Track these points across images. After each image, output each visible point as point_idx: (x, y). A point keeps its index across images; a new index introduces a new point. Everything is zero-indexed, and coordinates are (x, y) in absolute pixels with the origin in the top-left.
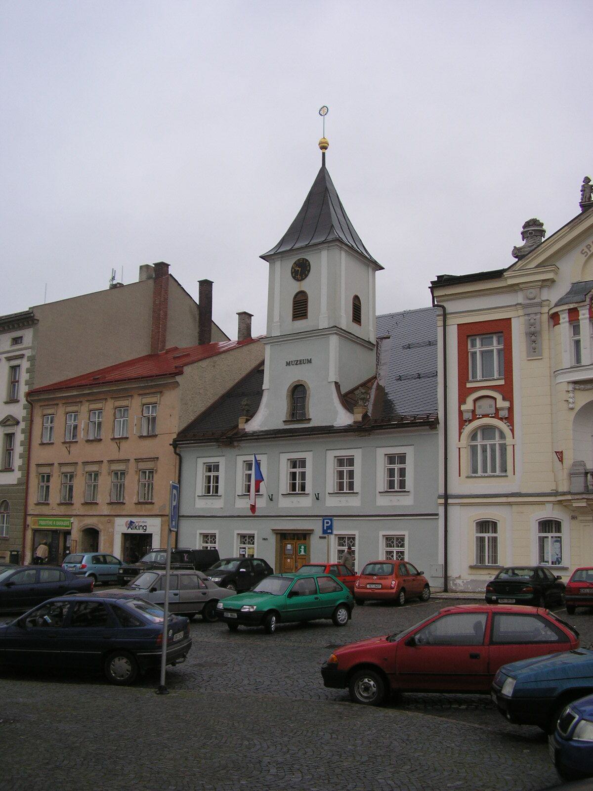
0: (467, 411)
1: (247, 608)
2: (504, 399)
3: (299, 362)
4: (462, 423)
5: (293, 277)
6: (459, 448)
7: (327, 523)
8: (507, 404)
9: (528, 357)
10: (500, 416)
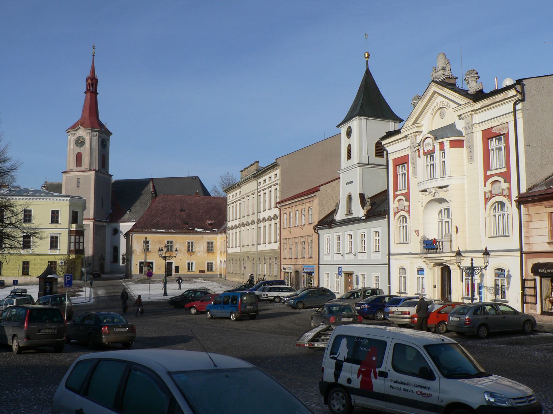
1: (406, 318)
2: (505, 182)
6: (485, 217)
7: (68, 278)
8: (506, 185)
9: (413, 176)
10: (504, 195)
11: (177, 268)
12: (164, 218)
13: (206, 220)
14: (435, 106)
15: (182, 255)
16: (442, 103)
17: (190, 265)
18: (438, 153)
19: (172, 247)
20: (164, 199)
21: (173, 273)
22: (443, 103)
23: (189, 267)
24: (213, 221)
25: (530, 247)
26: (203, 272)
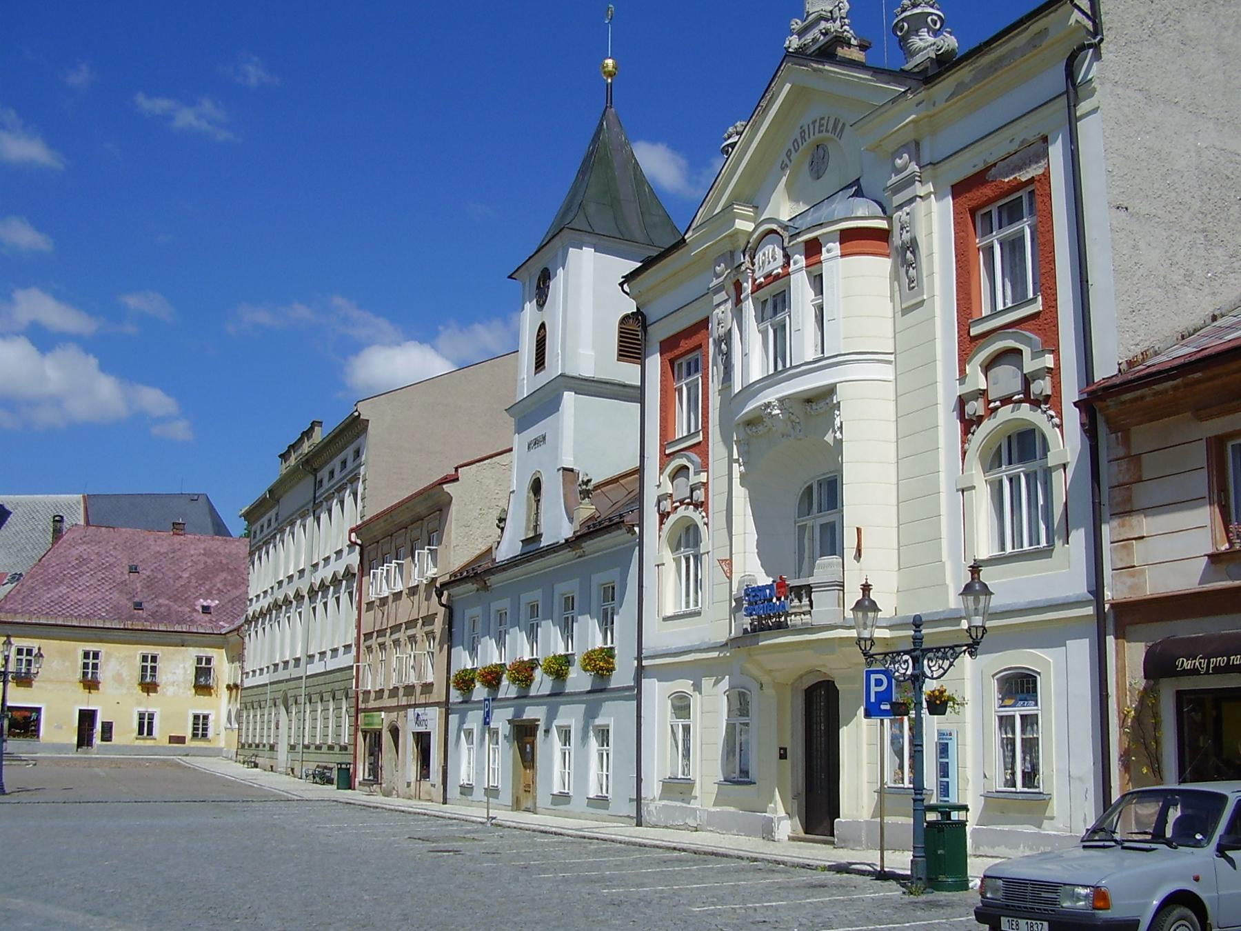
11: (107, 729)
12: (80, 588)
13: (197, 598)
14: (796, 140)
15: (124, 691)
16: (817, 124)
17: (144, 719)
18: (800, 286)
19: (97, 669)
20: (85, 537)
21: (97, 740)
22: (822, 122)
23: (141, 725)
24: (217, 602)
25: (1136, 580)
26: (181, 740)
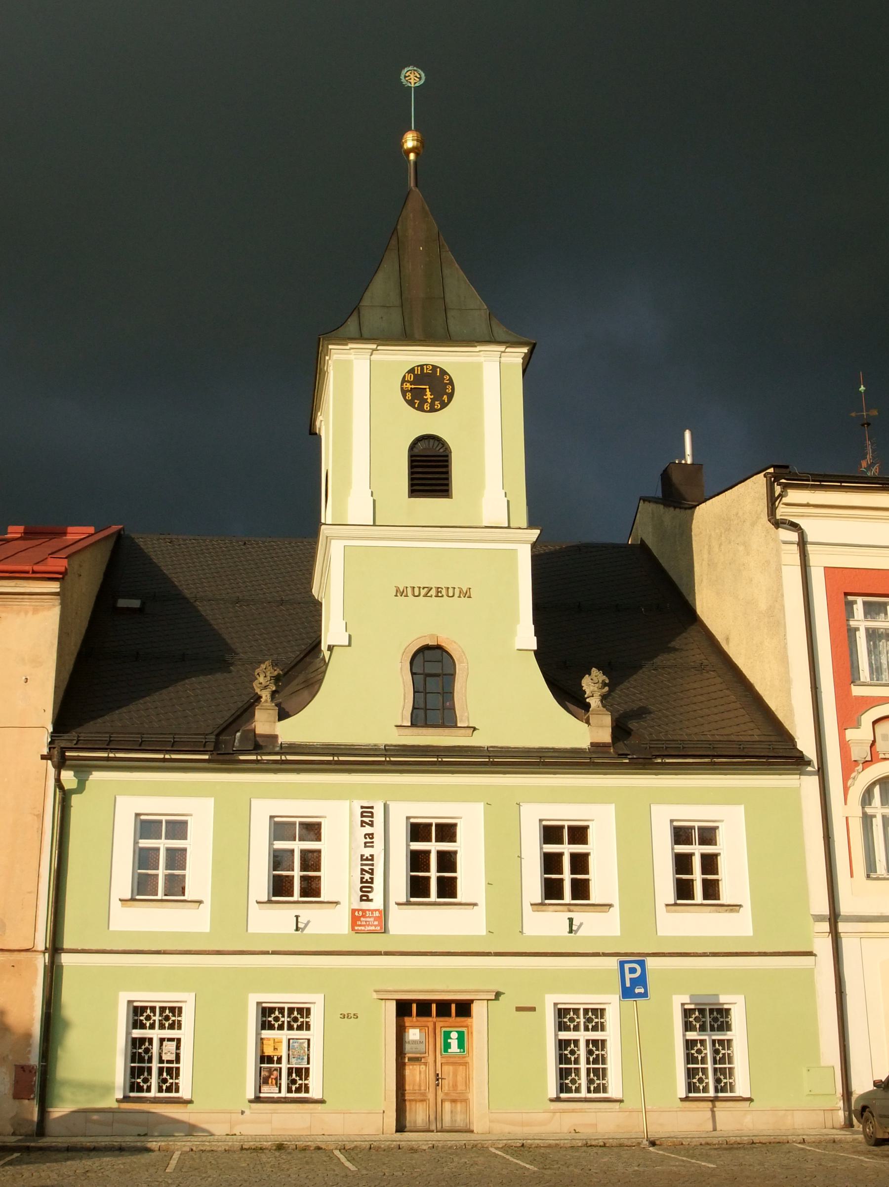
0: (860, 742)
3: (433, 592)
4: (849, 767)
5: (407, 401)
7: (633, 971)
